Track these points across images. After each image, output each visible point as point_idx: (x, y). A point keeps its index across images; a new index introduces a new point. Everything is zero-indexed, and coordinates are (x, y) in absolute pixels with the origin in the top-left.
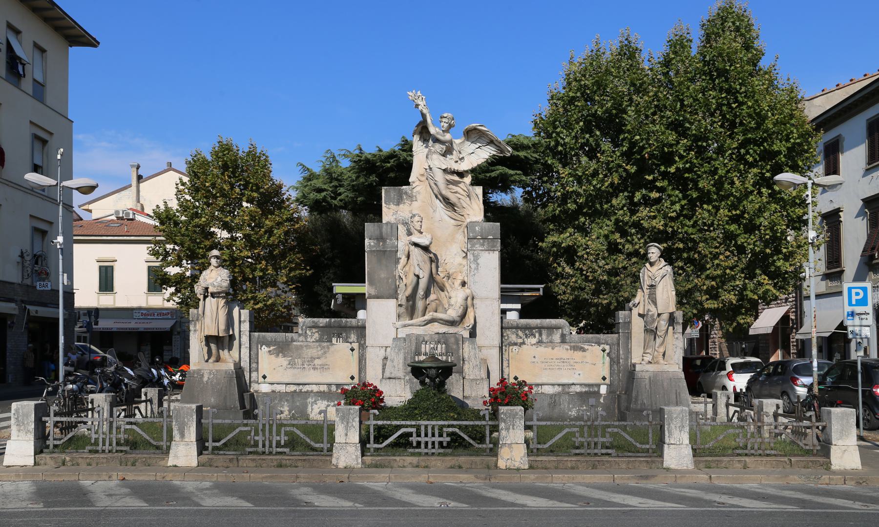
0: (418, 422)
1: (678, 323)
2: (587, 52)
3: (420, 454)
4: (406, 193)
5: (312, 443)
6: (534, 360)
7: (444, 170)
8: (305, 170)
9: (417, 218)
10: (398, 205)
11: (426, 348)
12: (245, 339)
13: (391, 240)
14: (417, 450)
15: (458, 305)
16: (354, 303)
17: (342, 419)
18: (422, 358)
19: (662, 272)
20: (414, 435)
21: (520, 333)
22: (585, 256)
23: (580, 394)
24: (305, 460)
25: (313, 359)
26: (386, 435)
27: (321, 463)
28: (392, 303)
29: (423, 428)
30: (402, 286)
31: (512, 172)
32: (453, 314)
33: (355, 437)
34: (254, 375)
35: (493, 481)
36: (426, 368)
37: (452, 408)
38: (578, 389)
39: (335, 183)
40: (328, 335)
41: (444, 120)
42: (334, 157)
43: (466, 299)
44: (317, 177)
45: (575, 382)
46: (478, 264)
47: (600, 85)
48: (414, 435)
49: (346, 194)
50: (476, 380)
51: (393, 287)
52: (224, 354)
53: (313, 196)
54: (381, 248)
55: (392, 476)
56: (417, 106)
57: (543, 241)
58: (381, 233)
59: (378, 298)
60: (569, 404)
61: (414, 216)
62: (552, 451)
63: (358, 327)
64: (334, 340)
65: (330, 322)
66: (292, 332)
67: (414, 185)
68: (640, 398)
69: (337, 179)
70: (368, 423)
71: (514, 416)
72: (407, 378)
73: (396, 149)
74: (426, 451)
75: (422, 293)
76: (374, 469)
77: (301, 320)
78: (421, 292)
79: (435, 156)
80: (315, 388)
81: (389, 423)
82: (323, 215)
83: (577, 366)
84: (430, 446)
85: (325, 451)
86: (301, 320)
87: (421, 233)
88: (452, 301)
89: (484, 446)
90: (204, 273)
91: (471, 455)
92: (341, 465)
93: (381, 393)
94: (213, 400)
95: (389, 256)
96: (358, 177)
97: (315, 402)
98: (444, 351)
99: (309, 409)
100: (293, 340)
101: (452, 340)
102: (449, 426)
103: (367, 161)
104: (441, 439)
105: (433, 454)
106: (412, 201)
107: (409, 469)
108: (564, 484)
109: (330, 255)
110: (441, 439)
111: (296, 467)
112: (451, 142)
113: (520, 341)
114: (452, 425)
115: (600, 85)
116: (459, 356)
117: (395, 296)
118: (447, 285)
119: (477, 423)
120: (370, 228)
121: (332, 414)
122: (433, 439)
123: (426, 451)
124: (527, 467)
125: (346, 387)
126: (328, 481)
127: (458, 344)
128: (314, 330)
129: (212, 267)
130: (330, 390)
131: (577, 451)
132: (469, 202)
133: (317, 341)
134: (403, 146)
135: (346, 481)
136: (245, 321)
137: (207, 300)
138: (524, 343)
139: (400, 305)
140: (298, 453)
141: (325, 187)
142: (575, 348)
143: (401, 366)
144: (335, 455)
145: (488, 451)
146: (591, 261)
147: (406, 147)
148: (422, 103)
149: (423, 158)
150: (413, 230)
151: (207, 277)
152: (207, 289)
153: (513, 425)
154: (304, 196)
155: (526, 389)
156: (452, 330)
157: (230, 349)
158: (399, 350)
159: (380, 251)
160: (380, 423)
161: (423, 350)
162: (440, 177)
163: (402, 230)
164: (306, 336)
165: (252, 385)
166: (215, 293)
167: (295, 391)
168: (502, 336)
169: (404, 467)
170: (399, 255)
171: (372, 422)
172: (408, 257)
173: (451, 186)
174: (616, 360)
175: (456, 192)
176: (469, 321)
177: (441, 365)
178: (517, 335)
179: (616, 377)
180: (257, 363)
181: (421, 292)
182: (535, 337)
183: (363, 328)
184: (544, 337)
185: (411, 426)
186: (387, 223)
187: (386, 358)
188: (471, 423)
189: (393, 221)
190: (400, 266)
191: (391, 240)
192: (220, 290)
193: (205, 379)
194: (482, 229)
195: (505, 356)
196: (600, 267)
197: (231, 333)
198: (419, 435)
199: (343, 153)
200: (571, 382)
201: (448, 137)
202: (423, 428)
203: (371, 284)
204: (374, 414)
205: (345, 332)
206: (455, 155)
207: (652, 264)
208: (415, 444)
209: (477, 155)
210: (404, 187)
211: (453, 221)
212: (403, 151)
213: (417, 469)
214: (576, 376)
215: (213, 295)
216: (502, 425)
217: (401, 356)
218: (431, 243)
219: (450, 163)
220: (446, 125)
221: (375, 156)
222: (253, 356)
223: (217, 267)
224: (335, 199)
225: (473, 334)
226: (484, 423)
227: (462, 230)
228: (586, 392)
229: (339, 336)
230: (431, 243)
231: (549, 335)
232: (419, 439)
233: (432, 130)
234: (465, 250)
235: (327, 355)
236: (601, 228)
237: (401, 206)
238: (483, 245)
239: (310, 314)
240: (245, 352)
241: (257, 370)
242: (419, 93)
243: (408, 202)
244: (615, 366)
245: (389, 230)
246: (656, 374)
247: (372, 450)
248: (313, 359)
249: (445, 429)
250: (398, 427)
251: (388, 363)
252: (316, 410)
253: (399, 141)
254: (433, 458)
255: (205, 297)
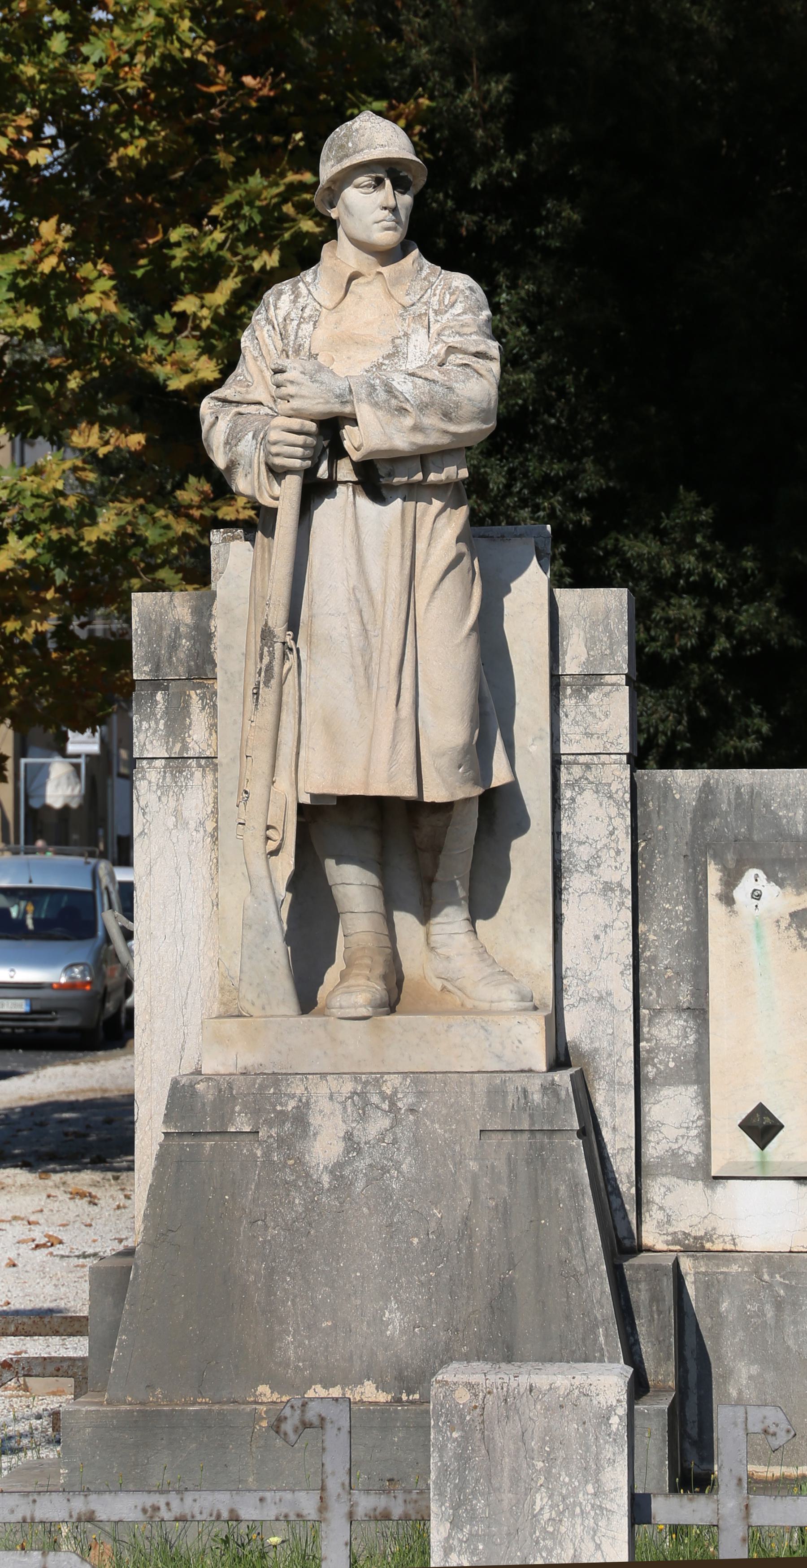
12: (598, 822)
34: (671, 1108)
52: (437, 946)
90: (280, 302)
94: (395, 1320)
109: (508, 165)
129: (339, 257)
136: (591, 680)
137: (329, 513)
151: (316, 337)
152: (330, 430)
157: (483, 904)
165: (655, 1190)
166: (397, 460)
180: (699, 1012)
192: (435, 433)
193: (324, 1148)
197: (500, 776)
215: (376, 479)
222: (662, 955)
223: (388, 256)
240: (598, 921)
241: (697, 1069)
255: (315, 491)
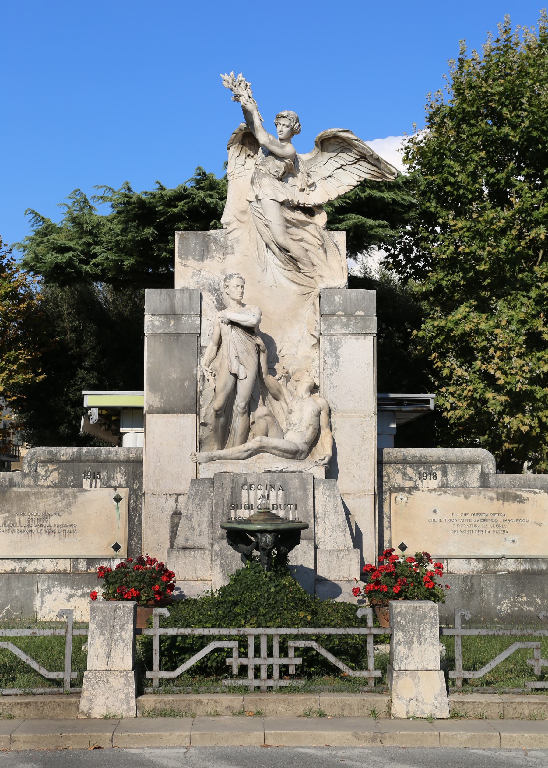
0: (242, 631)
2: (489, 44)
3: (246, 690)
4: (215, 241)
5: (43, 672)
6: (434, 516)
7: (282, 204)
8: (37, 221)
9: (235, 281)
10: (202, 259)
11: (252, 497)
13: (189, 316)
14: (241, 682)
15: (305, 424)
16: (113, 421)
17: (102, 626)
18: (244, 514)
20: (235, 654)
21: (410, 471)
23: (516, 575)
24: (27, 704)
25: (47, 515)
26: (180, 651)
27: (58, 710)
28: (190, 420)
29: (251, 642)
30: (208, 393)
31: (371, 222)
32: (296, 438)
33: (124, 659)
35: (387, 743)
36: (253, 533)
37: (300, 603)
38: (512, 566)
39: (88, 239)
40: (74, 476)
41: (282, 121)
42: (86, 200)
43: (319, 414)
44: (59, 230)
45: (506, 554)
46: (338, 357)
47: (512, 96)
48: (235, 654)
49: (103, 256)
50: (338, 551)
51: (192, 394)
53: (51, 257)
54: (172, 330)
55: (196, 734)
56: (237, 97)
57: (419, 329)
58: (173, 306)
59: (165, 412)
60: (496, 591)
61: (231, 276)
62: (489, 683)
63: (128, 462)
64: (86, 483)
65: (79, 453)
66: (8, 470)
67: (229, 229)
69: (90, 233)
70: (147, 632)
71: (422, 618)
72: (216, 547)
73: (188, 186)
74: (257, 683)
75: (243, 404)
76: (160, 720)
77: (24, 452)
78: (240, 402)
79: (266, 181)
80: (49, 566)
81: (187, 631)
82: (67, 288)
83: (509, 527)
84: (263, 673)
85: (67, 686)
86: (24, 452)
87: (243, 305)
88: (294, 418)
89: (365, 674)
91: (341, 691)
92: (98, 712)
93: (171, 575)
95: (189, 343)
96: (124, 231)
97: (49, 590)
98: (281, 501)
99: (38, 603)
100: (12, 484)
101: (295, 482)
102: (297, 637)
103: (141, 203)
104: (285, 661)
105: (270, 689)
106: (225, 254)
107: (227, 719)
108: (526, 752)
110: (285, 661)
111: (11, 717)
112: (295, 159)
113: (410, 484)
114: (306, 636)
115: (512, 96)
116: (307, 511)
117: (193, 407)
118: (284, 391)
119: (351, 631)
120: (152, 297)
121: (81, 608)
122: (270, 661)
123: (257, 683)
124: (446, 714)
125: (105, 564)
126: (71, 745)
127: (305, 489)
128: (51, 467)
130: (76, 569)
131: (539, 685)
132: (323, 256)
133: (55, 485)
134: (198, 182)
135: (107, 745)
138: (415, 488)
139: (204, 424)
140: (16, 690)
141: (71, 244)
142: (505, 497)
143: (205, 527)
144: (86, 694)
145: (372, 682)
147: (204, 183)
148: (245, 94)
149: (246, 183)
150: (227, 300)
153: (419, 637)
154: (37, 258)
155: (431, 567)
156: (294, 465)
158: (202, 500)
159: (170, 335)
160: (171, 631)
161: (244, 500)
162: (274, 214)
163: (209, 301)
164: (35, 475)
167: (13, 572)
168: (380, 476)
169: (216, 714)
170: (203, 341)
171: (156, 632)
172: (219, 344)
173: (293, 230)
175: (301, 240)
176: (323, 450)
177: (282, 526)
178: (405, 474)
181: (240, 402)
182: (435, 477)
183: (139, 462)
184: (451, 478)
185: (230, 638)
186: (183, 290)
187: (177, 514)
188: (341, 631)
189: (192, 285)
190: (204, 360)
191: (189, 316)
194: (345, 300)
195: (386, 510)
198: (244, 655)
199: (100, 193)
200: (499, 554)
201: (288, 149)
202: (251, 642)
203: (153, 389)
204: (161, 616)
205: (106, 469)
206: (299, 180)
208: (235, 671)
209: (334, 179)
210: (212, 231)
211: (294, 287)
212: (198, 189)
213: (240, 720)
214: (509, 544)
216: (399, 636)
217: (206, 509)
218: (259, 321)
219: (290, 190)
220: (286, 130)
221: (154, 195)
224: (87, 263)
225: (331, 471)
226: (363, 631)
227: (310, 301)
228: (525, 572)
229: (94, 476)
230: (259, 321)
231: (460, 474)
232: (244, 661)
233: (262, 137)
234: (317, 334)
235: (73, 509)
236: (514, 308)
237: (207, 262)
238: (347, 326)
239: (37, 441)
242: (240, 77)
243: (218, 256)
245: (186, 301)
247: (156, 682)
248: (47, 515)
249: (292, 643)
250: (203, 641)
251: (183, 522)
252: (54, 604)
253: (192, 174)
254: (270, 697)
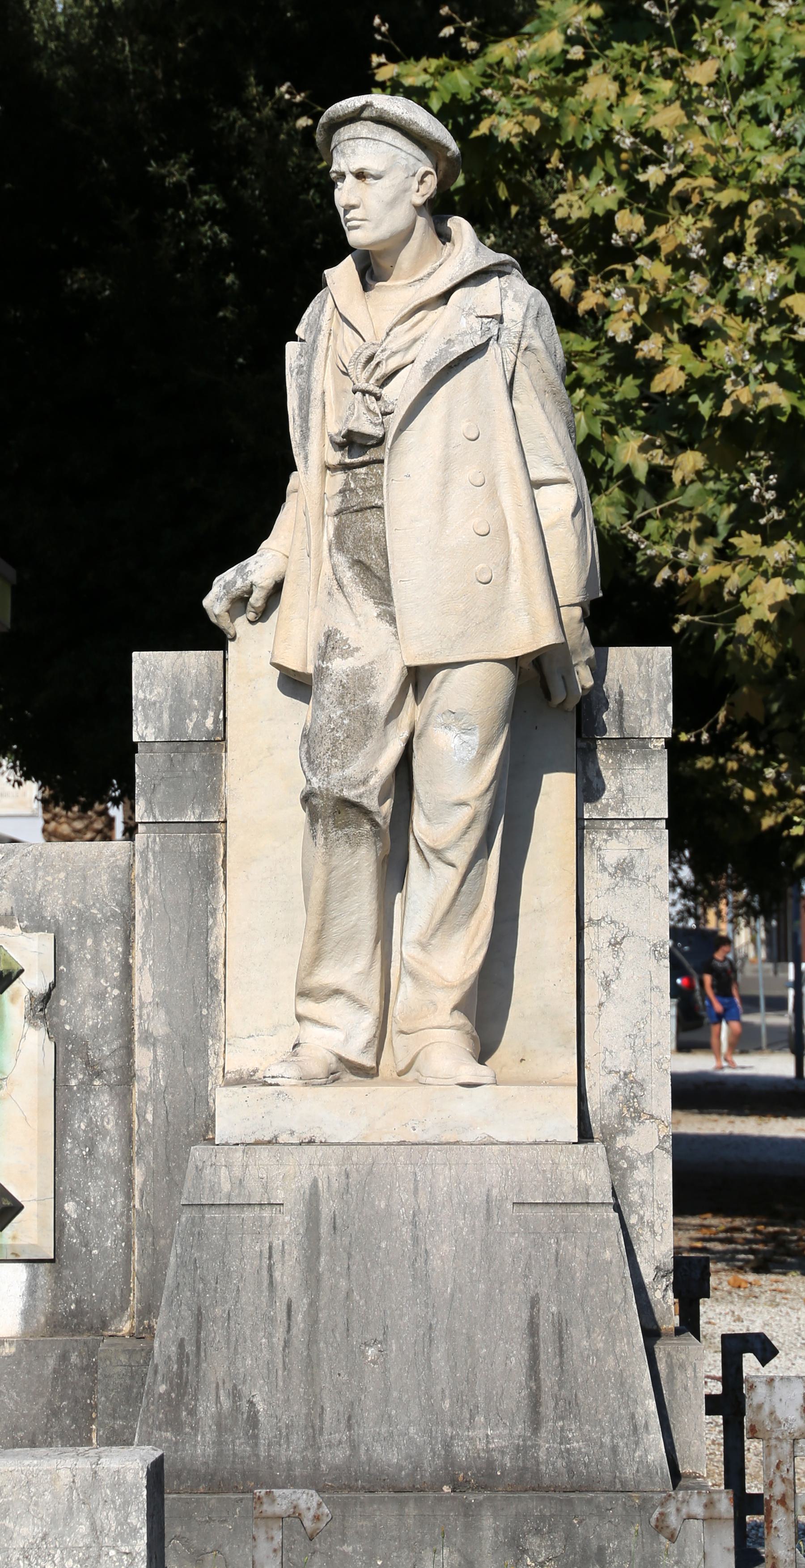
1: (631, 743)
19: (454, 326)
22: (630, 223)
68: (215, 1368)
146: (680, 260)
174: (106, 1050)
179: (101, 1189)
196: (745, 308)
207: (371, 272)
244: (103, 1105)
246: (363, 1169)
